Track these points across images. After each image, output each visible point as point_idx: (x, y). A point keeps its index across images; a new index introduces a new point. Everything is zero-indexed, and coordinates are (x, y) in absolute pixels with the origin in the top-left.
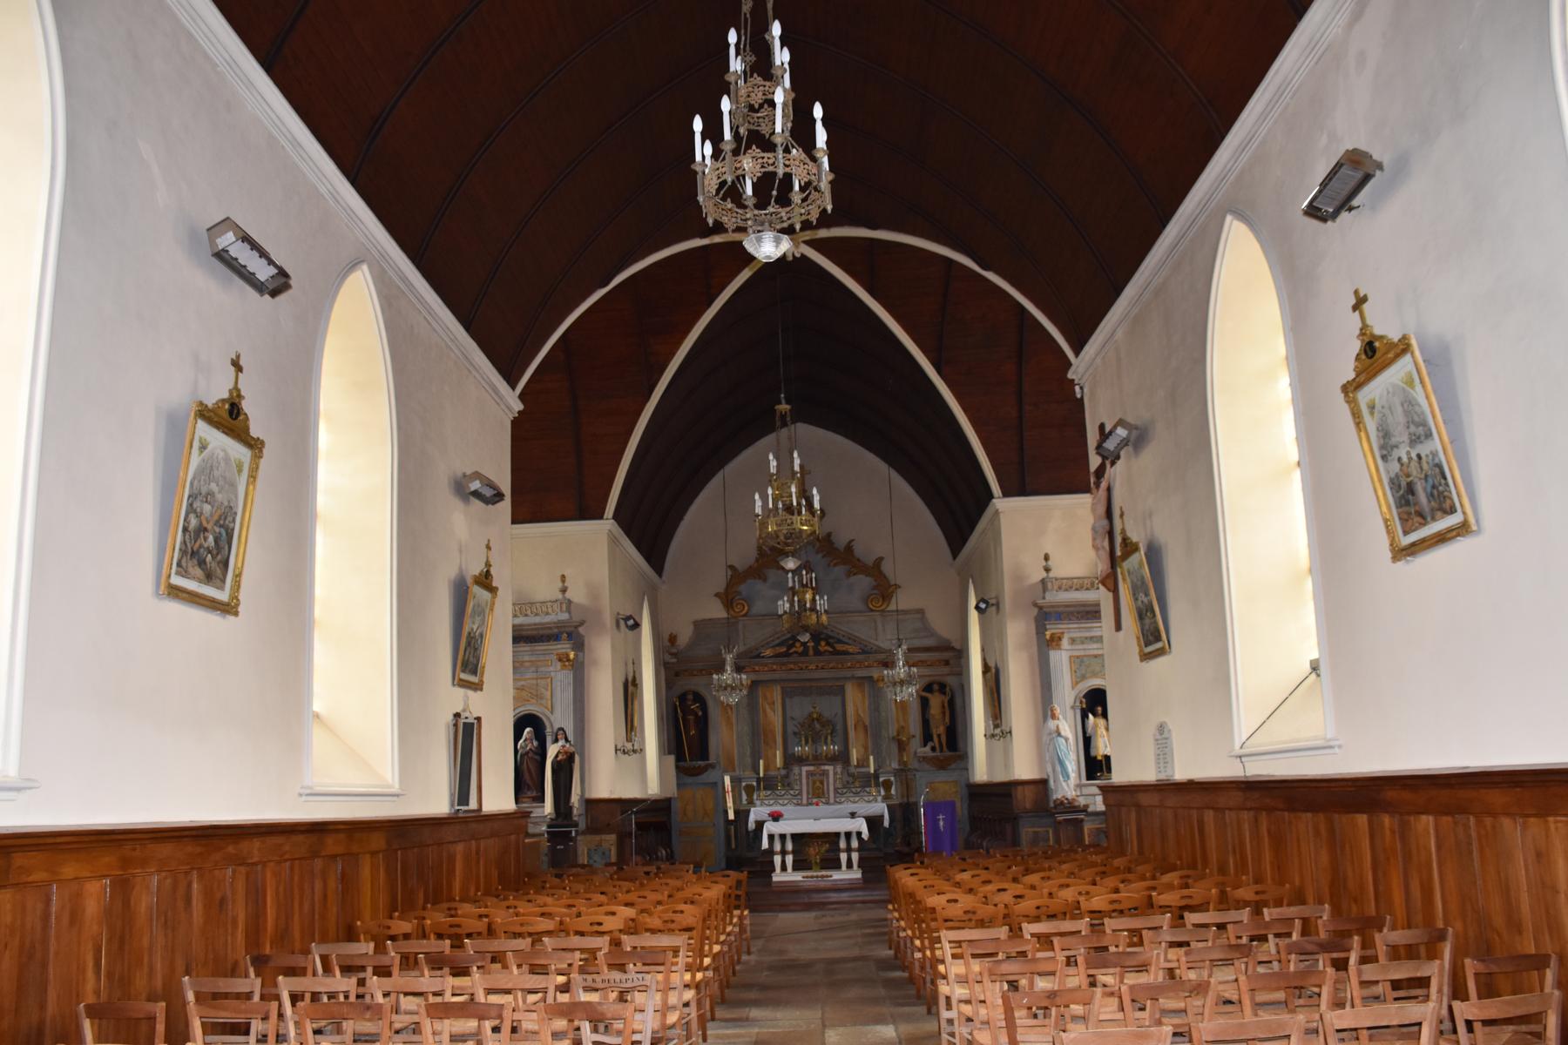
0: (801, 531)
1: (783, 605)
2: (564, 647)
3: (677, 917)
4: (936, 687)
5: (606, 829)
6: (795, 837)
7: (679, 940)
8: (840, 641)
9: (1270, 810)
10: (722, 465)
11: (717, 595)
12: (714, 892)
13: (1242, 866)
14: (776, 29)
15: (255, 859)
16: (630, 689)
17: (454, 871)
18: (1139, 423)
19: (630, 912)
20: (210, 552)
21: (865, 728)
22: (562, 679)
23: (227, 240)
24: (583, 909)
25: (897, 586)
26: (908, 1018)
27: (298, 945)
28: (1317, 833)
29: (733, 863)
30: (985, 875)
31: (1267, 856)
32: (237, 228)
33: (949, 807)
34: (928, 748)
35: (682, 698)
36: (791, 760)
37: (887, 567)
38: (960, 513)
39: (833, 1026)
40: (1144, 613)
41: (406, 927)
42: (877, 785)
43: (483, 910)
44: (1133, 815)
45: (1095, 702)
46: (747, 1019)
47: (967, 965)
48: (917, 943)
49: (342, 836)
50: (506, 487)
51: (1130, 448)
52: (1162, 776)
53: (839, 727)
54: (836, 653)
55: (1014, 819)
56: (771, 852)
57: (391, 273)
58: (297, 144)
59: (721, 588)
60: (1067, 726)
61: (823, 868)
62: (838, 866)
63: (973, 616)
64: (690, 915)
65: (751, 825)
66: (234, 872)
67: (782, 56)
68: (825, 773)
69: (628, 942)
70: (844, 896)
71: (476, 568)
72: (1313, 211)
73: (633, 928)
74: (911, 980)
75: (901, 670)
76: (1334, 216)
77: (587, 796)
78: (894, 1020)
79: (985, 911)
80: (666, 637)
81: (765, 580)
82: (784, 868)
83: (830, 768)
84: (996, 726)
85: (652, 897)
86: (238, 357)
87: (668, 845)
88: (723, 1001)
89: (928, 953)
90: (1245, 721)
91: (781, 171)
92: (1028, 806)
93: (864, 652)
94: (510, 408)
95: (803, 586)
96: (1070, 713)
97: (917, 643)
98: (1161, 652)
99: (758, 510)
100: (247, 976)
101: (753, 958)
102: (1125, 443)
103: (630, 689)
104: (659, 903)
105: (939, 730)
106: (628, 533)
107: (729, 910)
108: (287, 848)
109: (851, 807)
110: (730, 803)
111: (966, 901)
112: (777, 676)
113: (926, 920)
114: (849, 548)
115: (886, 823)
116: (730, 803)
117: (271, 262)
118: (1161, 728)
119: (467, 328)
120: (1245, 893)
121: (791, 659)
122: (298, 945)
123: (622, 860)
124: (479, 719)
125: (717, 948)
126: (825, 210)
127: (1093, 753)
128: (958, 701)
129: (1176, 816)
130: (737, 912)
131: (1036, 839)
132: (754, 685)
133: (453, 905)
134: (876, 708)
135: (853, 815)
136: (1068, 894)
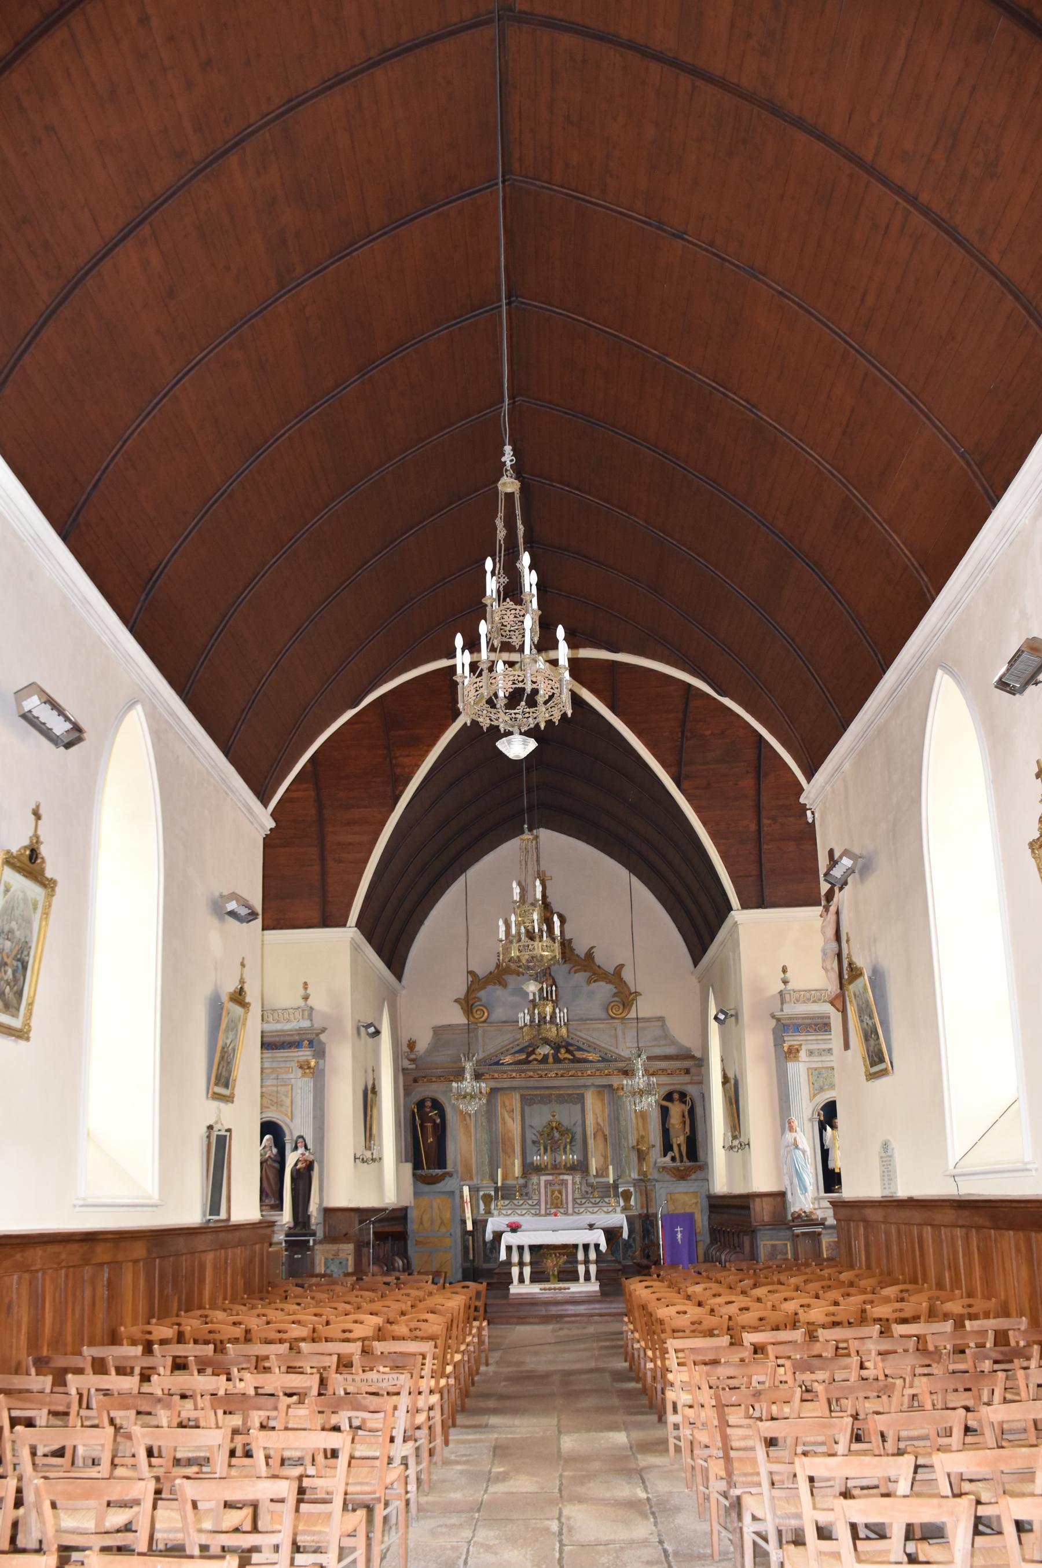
0: (542, 956)
1: (524, 1017)
2: (304, 1054)
3: (422, 1325)
4: (676, 1096)
5: (345, 1238)
6: (532, 1248)
7: (427, 1347)
8: (579, 1049)
9: (979, 1228)
10: (463, 870)
11: (456, 1001)
12: (455, 1301)
13: (956, 1283)
14: (526, 559)
15: (38, 1267)
16: (369, 1096)
17: (204, 1278)
18: (864, 853)
19: (377, 1320)
20: (8, 984)
21: (605, 1136)
22: (302, 1087)
23: (32, 703)
24: (332, 1318)
25: (637, 994)
26: (639, 1426)
27: (69, 1349)
28: (1018, 1250)
29: (471, 1274)
30: (715, 1287)
31: (977, 1272)
32: (42, 692)
33: (688, 1219)
34: (668, 1158)
35: (421, 1104)
36: (530, 1169)
37: (627, 975)
38: (700, 921)
39: (569, 1432)
40: (870, 1035)
41: (167, 1332)
42: (616, 1195)
43: (235, 1318)
44: (862, 1230)
45: (829, 1115)
46: (486, 1426)
47: (690, 1371)
48: (650, 1353)
49: (109, 1244)
50: (258, 907)
51: (857, 875)
52: (887, 1193)
53: (579, 1136)
54: (576, 1060)
55: (752, 1233)
56: (508, 1263)
57: (161, 710)
58: (86, 602)
59: (461, 993)
60: (805, 1138)
61: (560, 1280)
62: (576, 1279)
63: (714, 1027)
64: (435, 1324)
65: (489, 1236)
66: (20, 1279)
67: (530, 579)
68: (564, 1183)
69: (379, 1347)
70: (582, 1309)
71: (230, 986)
72: (1002, 684)
73: (380, 1334)
74: (644, 1391)
75: (640, 1080)
76: (1021, 690)
77: (326, 1204)
78: (626, 1427)
79: (709, 1322)
80: (405, 1042)
81: (505, 986)
82: (521, 1280)
83: (569, 1178)
84: (734, 1137)
85: (396, 1306)
86: (38, 807)
87: (404, 1254)
88: (463, 1409)
89: (659, 1363)
90: (958, 1141)
91: (529, 689)
92: (766, 1218)
93: (604, 1060)
94: (262, 827)
95: (541, 998)
96: (808, 1126)
97: (658, 1051)
98: (884, 1073)
99: (502, 935)
100: (28, 1374)
101: (491, 1369)
102: (851, 871)
103: (369, 1096)
104: (403, 1314)
105: (679, 1140)
106: (370, 940)
107: (468, 1320)
108: (63, 1256)
109: (589, 1218)
110: (468, 1215)
111: (694, 1312)
112: (515, 1083)
113: (655, 1330)
114: (590, 955)
115: (625, 1235)
116: (468, 1215)
117: (67, 719)
118: (886, 1146)
119: (226, 754)
120: (955, 1307)
121: (530, 1066)
122: (69, 1349)
123: (359, 1272)
124: (229, 1130)
125: (458, 1357)
126: (564, 715)
127: (831, 1166)
128: (699, 1110)
129: (899, 1231)
130: (476, 1324)
131: (773, 1253)
132: (493, 1091)
133: (206, 1312)
134: (616, 1119)
135: (591, 1227)
136: (791, 1306)
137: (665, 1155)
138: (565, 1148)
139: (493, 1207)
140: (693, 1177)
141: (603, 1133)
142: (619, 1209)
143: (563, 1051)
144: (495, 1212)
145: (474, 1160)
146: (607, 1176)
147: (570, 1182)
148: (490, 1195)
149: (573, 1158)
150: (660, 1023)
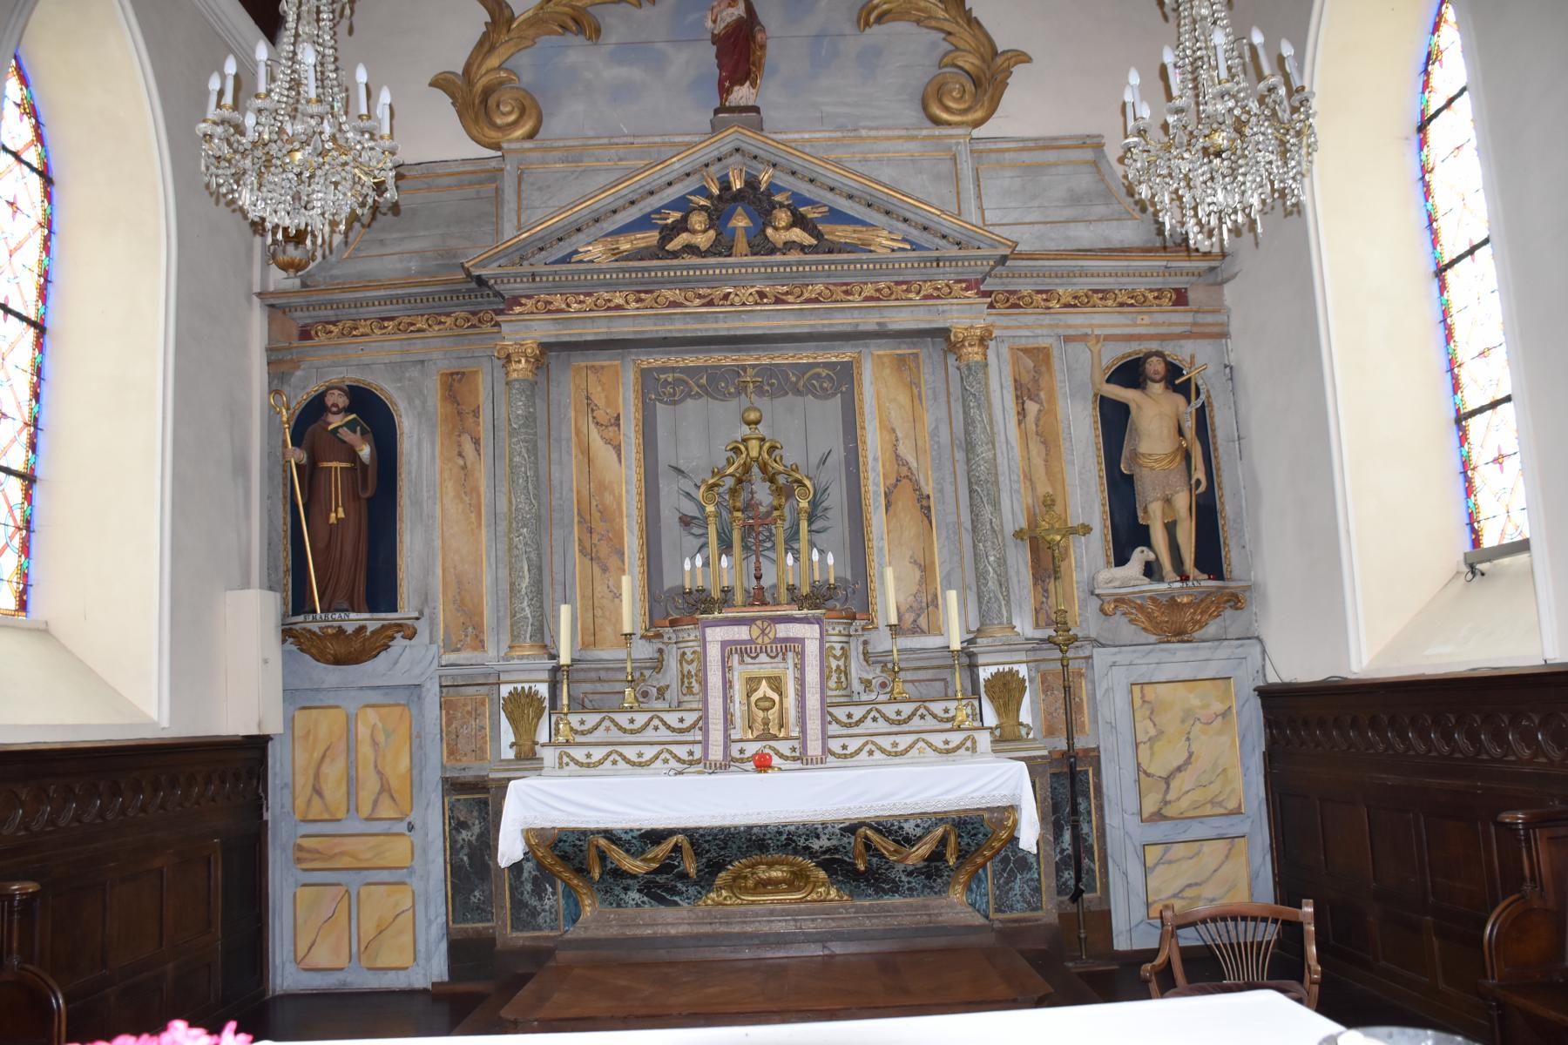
36: (679, 609)
53: (836, 499)
115: (1029, 834)
128: (1221, 420)
137: (1121, 559)
138: (793, 535)
139: (543, 735)
140: (1212, 629)
141: (917, 489)
142: (984, 739)
143: (783, 217)
144: (549, 755)
145: (487, 581)
146: (935, 629)
147: (812, 648)
148: (532, 697)
149: (827, 563)
150: (1089, 155)
